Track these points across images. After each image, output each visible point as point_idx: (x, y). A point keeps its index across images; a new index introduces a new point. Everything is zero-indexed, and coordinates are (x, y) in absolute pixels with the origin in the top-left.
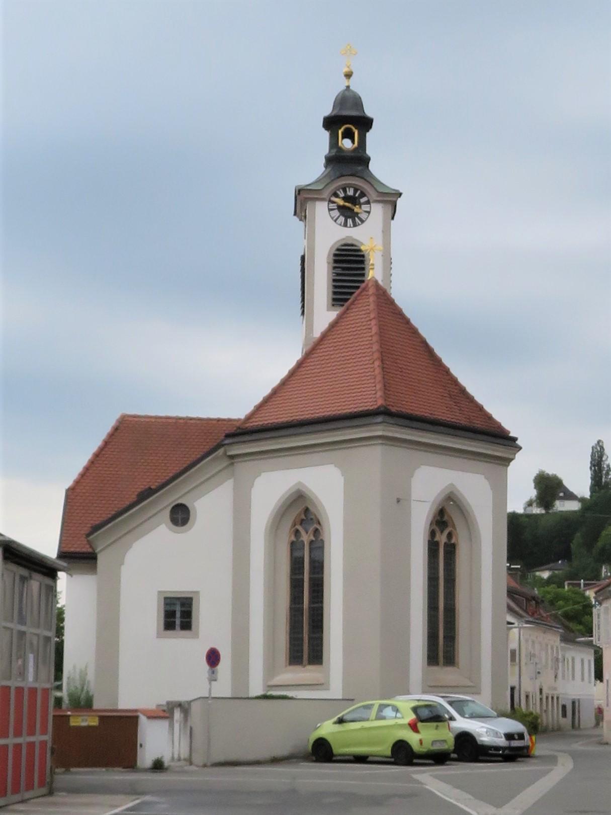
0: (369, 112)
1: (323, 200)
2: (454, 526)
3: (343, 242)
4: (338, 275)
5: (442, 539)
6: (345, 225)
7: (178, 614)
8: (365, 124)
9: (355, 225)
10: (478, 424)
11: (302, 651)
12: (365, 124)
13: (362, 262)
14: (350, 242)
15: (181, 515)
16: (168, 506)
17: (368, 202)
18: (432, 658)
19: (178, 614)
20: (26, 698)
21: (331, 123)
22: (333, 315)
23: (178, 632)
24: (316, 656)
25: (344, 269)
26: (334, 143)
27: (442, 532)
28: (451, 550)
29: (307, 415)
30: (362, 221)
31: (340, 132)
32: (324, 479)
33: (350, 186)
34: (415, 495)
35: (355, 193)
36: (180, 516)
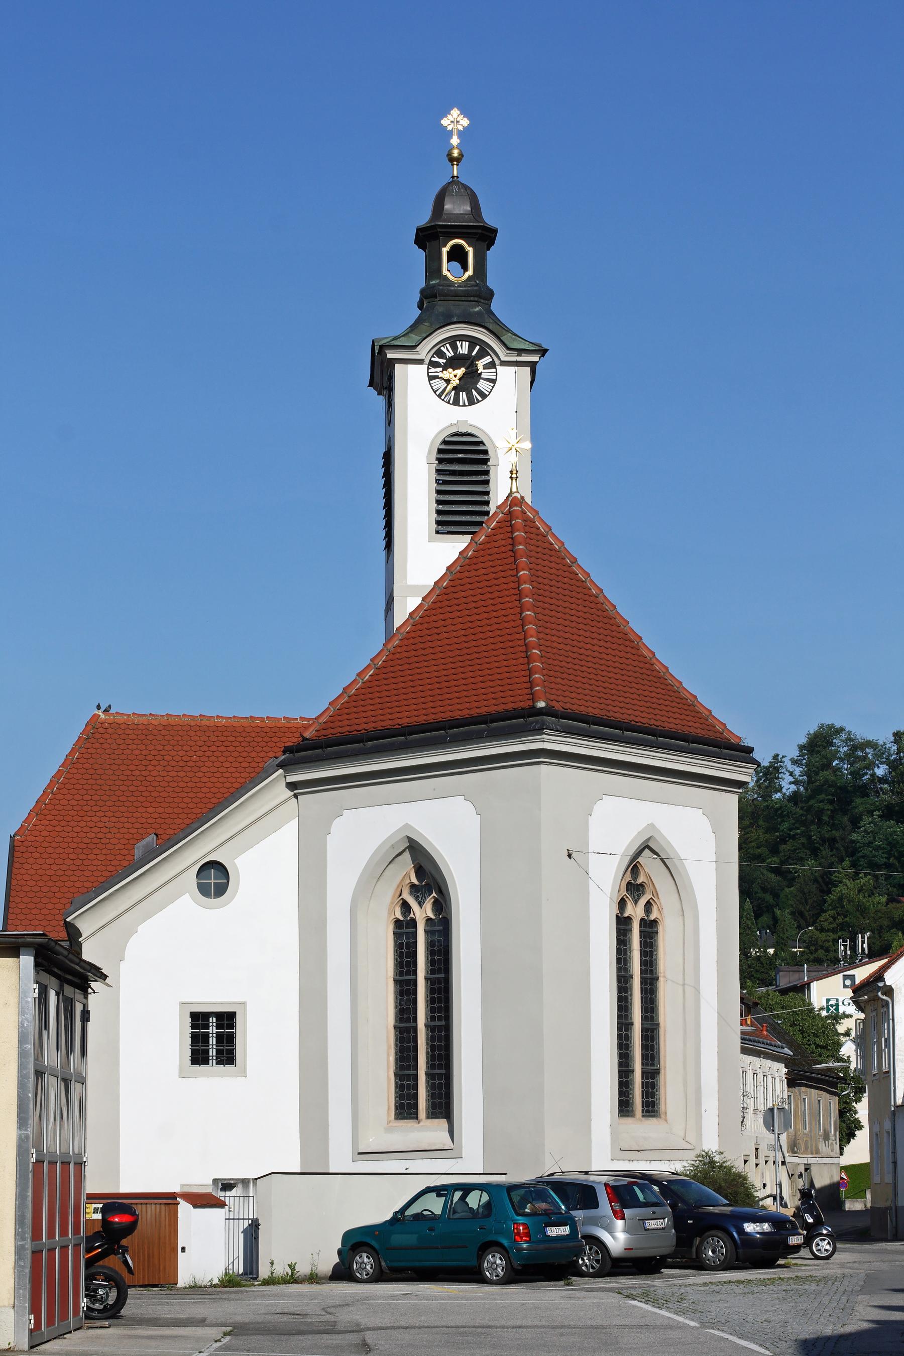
0: (490, 219)
1: (420, 362)
2: (655, 893)
3: (454, 430)
4: (445, 482)
5: (636, 912)
6: (456, 402)
7: (213, 1038)
8: (485, 237)
9: (472, 402)
10: (695, 730)
11: (416, 1096)
12: (485, 237)
13: (486, 461)
14: (463, 430)
15: (214, 879)
16: (194, 863)
17: (492, 365)
18: (624, 1107)
19: (213, 1038)
20: (481, 456)
21: (428, 238)
22: (453, 547)
23: (213, 1068)
24: (443, 1106)
25: (453, 473)
26: (433, 269)
27: (636, 902)
28: (650, 928)
29: (388, 722)
30: (484, 396)
31: (445, 250)
32: (447, 814)
33: (462, 338)
34: (595, 842)
35: (471, 349)
36: (213, 879)
